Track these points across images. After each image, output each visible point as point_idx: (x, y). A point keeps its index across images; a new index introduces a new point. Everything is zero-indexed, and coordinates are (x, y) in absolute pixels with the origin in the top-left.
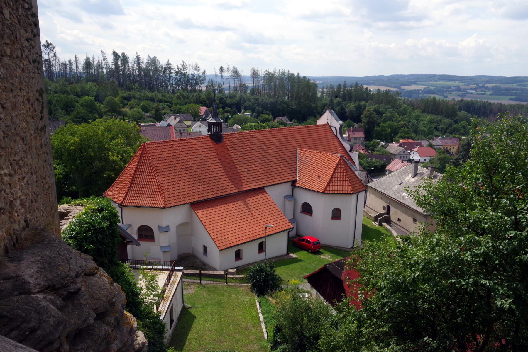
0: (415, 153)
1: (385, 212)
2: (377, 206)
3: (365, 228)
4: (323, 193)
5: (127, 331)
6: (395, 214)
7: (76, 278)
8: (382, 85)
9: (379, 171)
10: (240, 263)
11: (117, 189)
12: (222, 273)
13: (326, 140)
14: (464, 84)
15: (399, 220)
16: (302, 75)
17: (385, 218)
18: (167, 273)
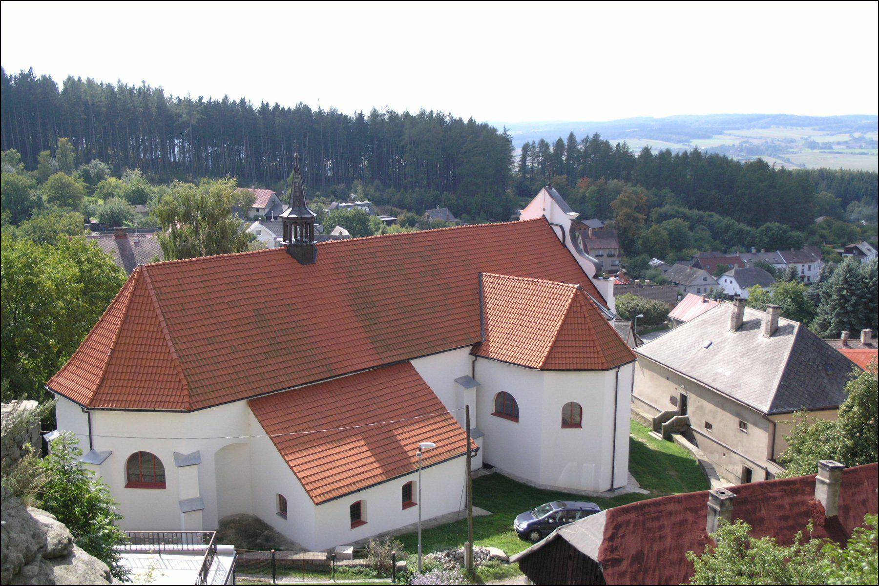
0: (729, 279)
1: (675, 409)
2: (658, 398)
3: (636, 448)
4: (542, 369)
5: (670, 578)
6: (699, 412)
7: (27, 564)
8: (650, 139)
9: (656, 322)
10: (361, 533)
11: (73, 377)
12: (322, 556)
13: (542, 254)
14: (821, 133)
15: (708, 426)
16: (479, 121)
17: (676, 425)
18: (201, 559)
